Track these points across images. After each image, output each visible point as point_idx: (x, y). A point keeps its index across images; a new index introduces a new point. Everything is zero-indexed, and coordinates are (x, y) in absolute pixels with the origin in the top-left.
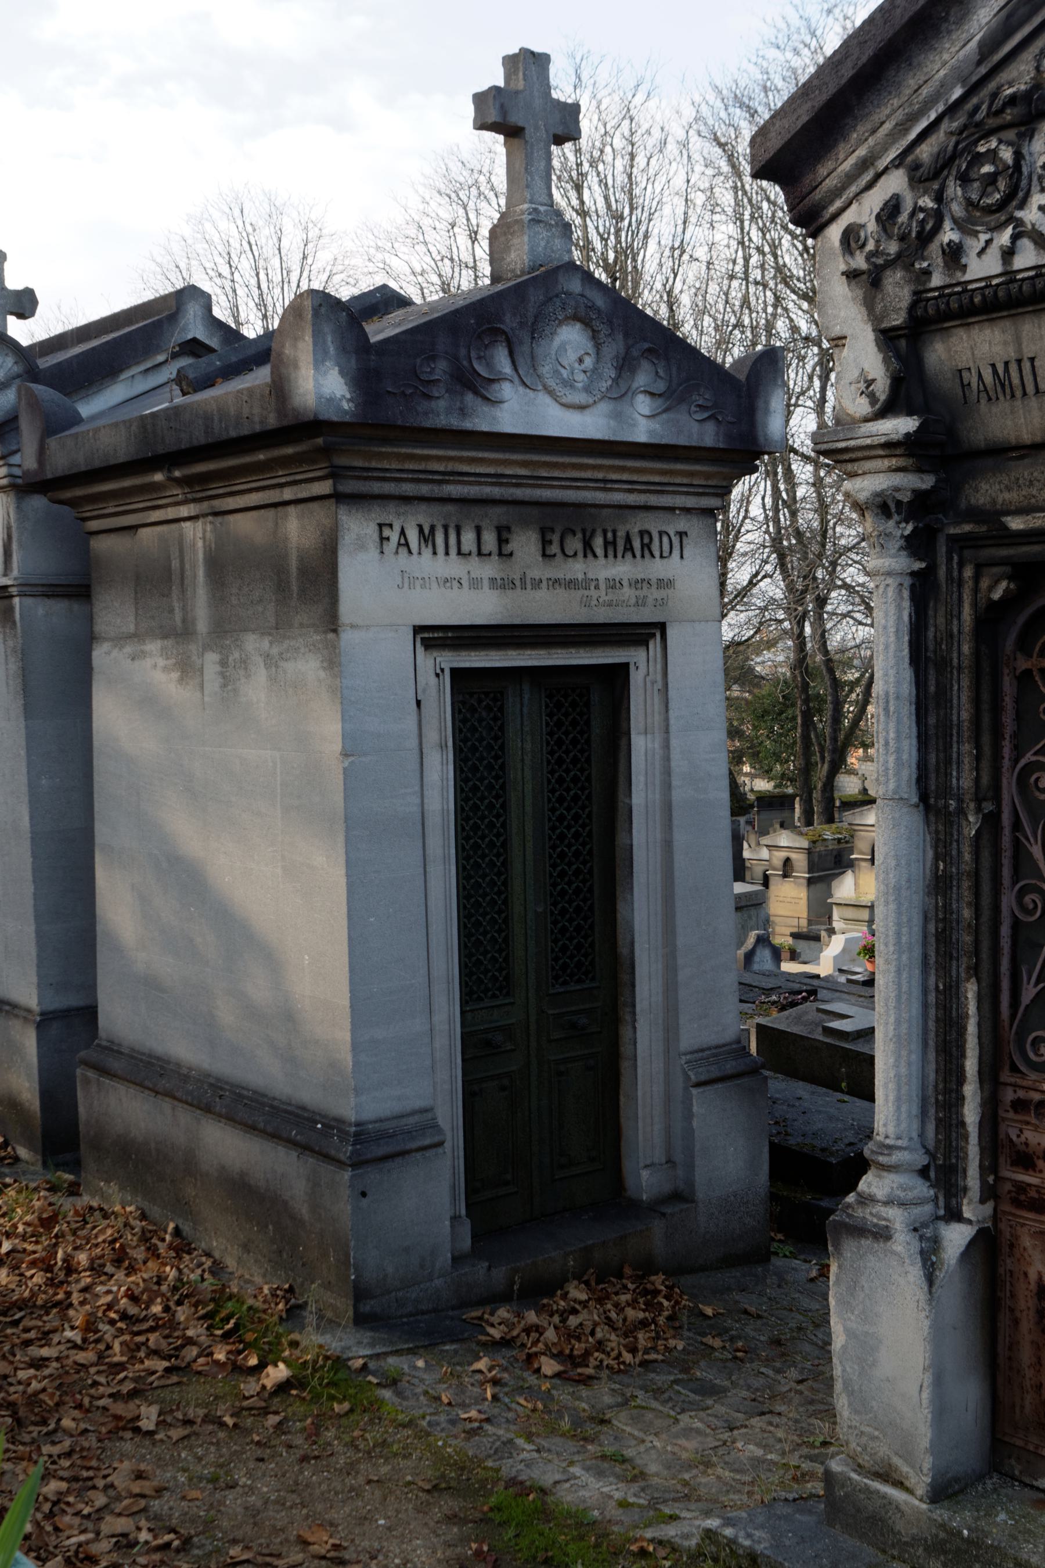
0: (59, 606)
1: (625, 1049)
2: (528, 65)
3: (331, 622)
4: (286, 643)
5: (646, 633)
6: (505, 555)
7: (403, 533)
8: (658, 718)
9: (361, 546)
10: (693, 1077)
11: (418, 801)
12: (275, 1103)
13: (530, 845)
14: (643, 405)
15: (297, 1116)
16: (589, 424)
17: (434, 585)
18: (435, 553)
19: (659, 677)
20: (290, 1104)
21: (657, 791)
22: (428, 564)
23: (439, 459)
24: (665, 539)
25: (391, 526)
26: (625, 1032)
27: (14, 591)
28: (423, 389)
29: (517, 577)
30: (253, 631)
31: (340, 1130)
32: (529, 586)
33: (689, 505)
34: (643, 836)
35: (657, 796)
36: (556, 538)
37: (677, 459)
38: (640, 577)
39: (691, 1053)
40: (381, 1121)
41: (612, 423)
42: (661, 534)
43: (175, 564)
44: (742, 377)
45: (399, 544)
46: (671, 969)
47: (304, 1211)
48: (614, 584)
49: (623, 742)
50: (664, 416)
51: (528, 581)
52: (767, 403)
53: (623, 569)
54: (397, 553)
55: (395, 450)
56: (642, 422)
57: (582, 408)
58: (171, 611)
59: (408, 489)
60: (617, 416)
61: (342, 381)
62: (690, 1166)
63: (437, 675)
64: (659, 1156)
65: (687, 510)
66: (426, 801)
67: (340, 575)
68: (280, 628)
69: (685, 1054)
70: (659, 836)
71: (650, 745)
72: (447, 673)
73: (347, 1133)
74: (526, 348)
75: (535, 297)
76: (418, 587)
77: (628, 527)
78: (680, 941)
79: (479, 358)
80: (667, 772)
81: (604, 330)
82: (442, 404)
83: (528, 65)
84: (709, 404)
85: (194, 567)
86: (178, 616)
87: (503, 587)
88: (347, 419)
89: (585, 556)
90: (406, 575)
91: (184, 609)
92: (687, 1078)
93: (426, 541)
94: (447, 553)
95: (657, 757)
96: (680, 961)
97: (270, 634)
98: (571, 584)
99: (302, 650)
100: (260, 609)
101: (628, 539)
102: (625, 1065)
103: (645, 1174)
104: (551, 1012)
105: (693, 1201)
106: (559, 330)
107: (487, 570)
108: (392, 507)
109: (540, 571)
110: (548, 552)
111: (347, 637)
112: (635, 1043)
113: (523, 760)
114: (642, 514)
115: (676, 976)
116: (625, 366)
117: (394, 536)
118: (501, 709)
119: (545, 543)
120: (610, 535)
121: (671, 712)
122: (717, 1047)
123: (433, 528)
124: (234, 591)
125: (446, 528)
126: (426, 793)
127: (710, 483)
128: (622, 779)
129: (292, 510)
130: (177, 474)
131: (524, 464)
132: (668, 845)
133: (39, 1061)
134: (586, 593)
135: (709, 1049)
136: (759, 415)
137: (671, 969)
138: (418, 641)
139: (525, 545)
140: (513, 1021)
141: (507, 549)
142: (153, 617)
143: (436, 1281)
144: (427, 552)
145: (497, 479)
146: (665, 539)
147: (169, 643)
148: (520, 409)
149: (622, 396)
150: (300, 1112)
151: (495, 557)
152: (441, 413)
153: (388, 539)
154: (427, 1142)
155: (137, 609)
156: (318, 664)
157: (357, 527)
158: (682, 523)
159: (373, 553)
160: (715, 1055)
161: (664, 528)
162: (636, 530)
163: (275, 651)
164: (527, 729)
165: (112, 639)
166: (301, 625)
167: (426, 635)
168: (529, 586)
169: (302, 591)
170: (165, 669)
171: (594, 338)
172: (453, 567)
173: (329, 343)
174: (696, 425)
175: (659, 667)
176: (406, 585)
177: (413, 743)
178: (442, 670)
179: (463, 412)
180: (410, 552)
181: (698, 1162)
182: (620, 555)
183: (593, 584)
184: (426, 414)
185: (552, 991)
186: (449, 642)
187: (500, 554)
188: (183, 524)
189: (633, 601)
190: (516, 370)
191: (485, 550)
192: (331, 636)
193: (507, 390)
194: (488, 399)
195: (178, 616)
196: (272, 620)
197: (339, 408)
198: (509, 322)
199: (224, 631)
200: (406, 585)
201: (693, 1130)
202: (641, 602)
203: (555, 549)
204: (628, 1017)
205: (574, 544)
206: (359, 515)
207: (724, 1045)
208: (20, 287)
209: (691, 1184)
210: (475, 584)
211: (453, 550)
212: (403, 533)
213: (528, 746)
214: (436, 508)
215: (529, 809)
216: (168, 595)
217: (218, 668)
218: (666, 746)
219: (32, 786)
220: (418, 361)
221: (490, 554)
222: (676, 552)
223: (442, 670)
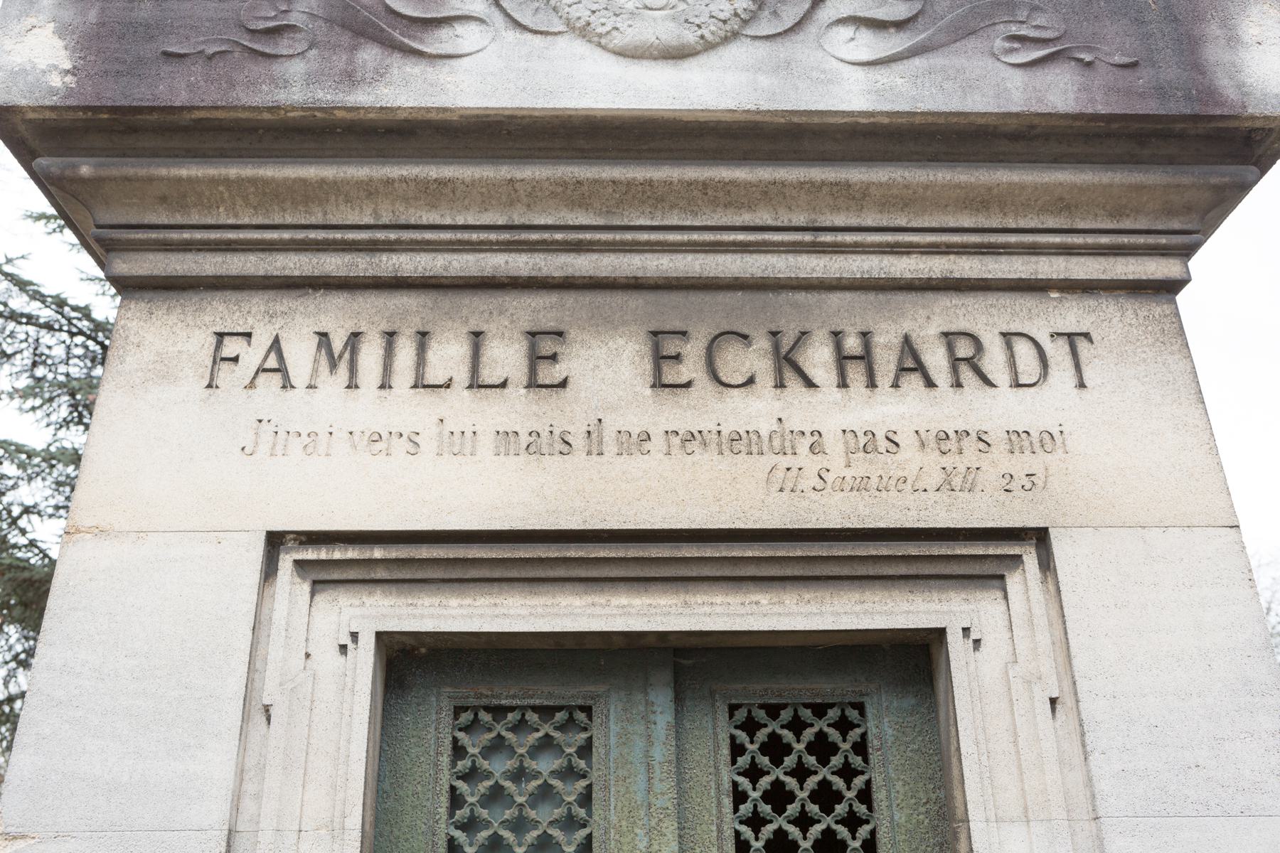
7: (276, 346)
22: (327, 403)
36: (693, 351)
48: (867, 443)
72: (367, 645)
93: (333, 365)
98: (738, 442)
107: (516, 410)
119: (660, 359)
125: (390, 336)
127: (1127, 224)
151: (517, 392)
162: (933, 329)
167: (310, 554)
172: (406, 409)
175: (1044, 639)
176: (264, 448)
182: (884, 380)
186: (381, 574)
189: (936, 478)
200: (264, 448)
203: (691, 368)
205: (753, 359)
221: (503, 385)
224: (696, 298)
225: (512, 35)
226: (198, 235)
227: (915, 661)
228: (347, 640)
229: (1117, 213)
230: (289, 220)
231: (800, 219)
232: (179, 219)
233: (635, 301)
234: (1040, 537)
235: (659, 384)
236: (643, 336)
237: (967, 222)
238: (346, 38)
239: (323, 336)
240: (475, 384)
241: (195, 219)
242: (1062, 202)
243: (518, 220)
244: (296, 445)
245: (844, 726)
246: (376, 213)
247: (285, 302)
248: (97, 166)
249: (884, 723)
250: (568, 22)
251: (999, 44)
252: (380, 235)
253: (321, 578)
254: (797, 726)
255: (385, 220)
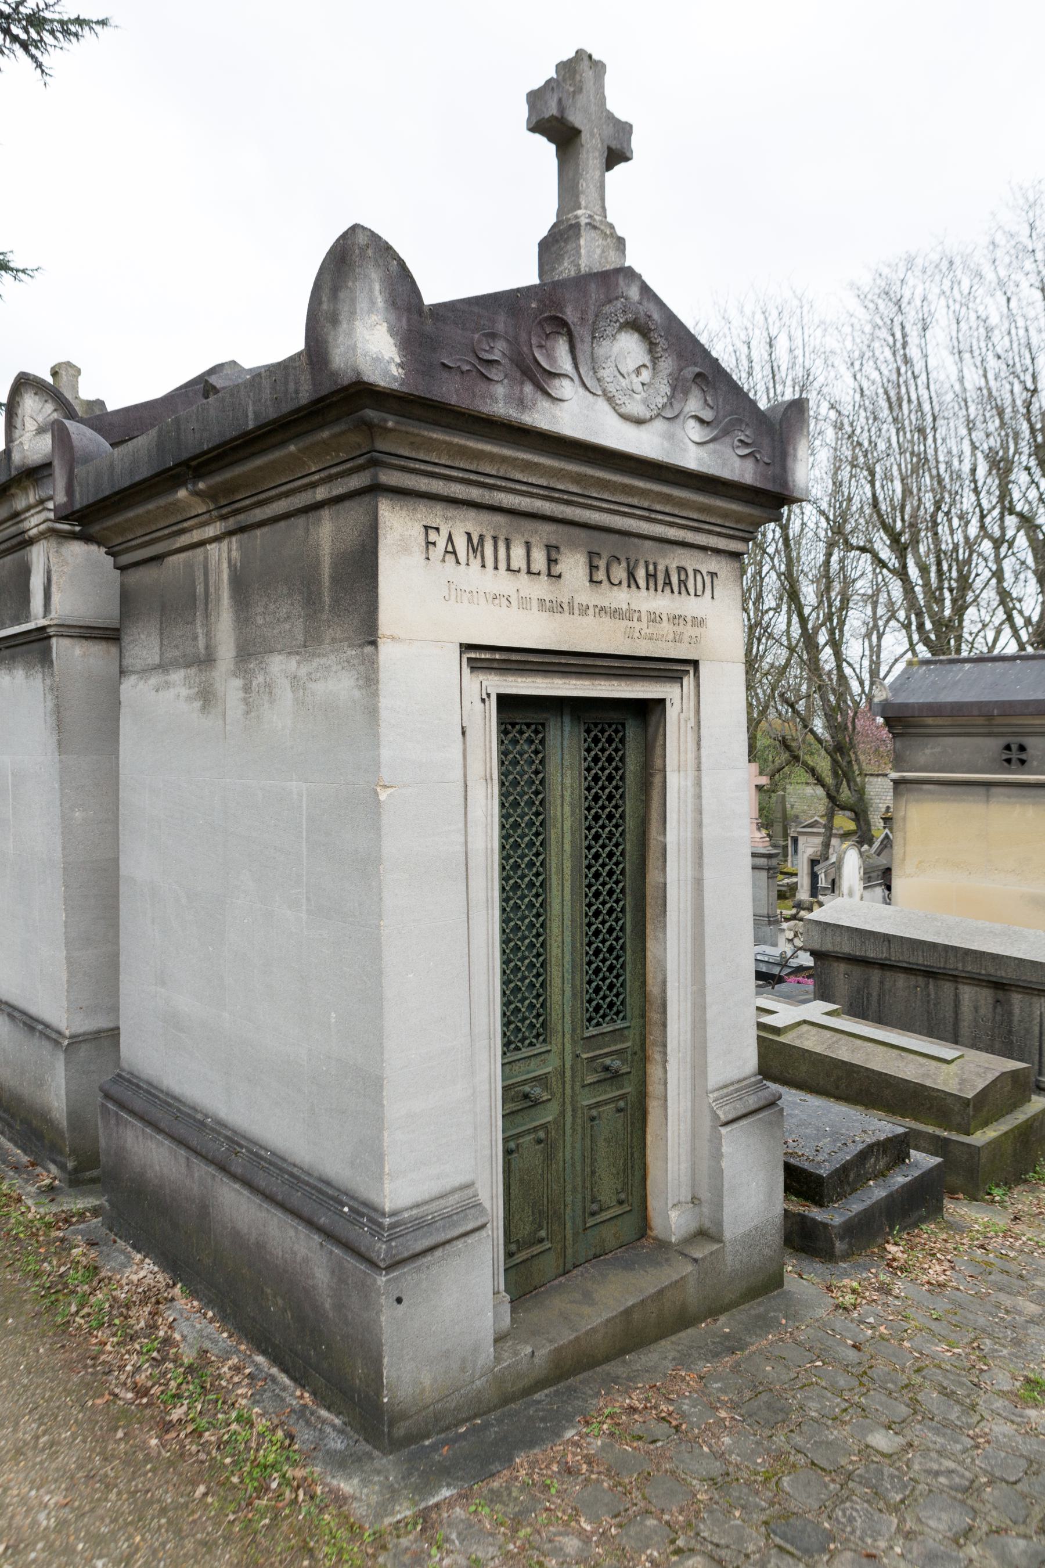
0: (97, 649)
1: (653, 1088)
2: (579, 72)
3: (368, 633)
4: (316, 662)
5: (676, 669)
6: (554, 577)
7: (450, 538)
8: (691, 756)
9: (405, 548)
10: (722, 1116)
11: (463, 839)
12: (295, 1170)
13: (568, 884)
14: (694, 431)
15: (320, 1191)
16: (643, 443)
17: (482, 600)
18: (483, 566)
19: (692, 714)
20: (309, 1174)
21: (689, 829)
22: (475, 577)
23: (492, 458)
24: (699, 577)
25: (437, 529)
26: (654, 1071)
27: (51, 631)
28: (482, 369)
29: (565, 600)
30: (279, 652)
31: (371, 1220)
32: (576, 612)
33: (720, 547)
34: (676, 875)
35: (689, 834)
36: (602, 564)
37: (716, 494)
38: (677, 613)
39: (717, 1090)
40: (417, 1206)
41: (666, 444)
42: (696, 571)
43: (200, 589)
44: (779, 416)
45: (446, 552)
46: (699, 1007)
47: (327, 1306)
48: (655, 618)
49: (657, 779)
50: (711, 445)
51: (576, 606)
52: (795, 449)
53: (662, 603)
54: (443, 561)
55: (447, 438)
56: (689, 448)
57: (639, 422)
58: (195, 638)
59: (458, 490)
60: (671, 437)
61: (392, 341)
62: (719, 1206)
63: (483, 700)
64: (685, 1195)
65: (717, 551)
66: (470, 839)
67: (381, 578)
68: (310, 643)
69: (712, 1092)
70: (690, 873)
71: (683, 783)
72: (494, 698)
73: (380, 1225)
74: (586, 347)
75: (595, 292)
76: (466, 601)
77: (667, 561)
78: (709, 978)
79: (541, 346)
80: (699, 810)
81: (662, 343)
82: (500, 390)
83: (579, 72)
84: (749, 441)
85: (218, 589)
86: (201, 643)
87: (552, 610)
88: (395, 386)
89: (629, 586)
90: (453, 587)
91: (208, 635)
92: (716, 1117)
93: (475, 551)
94: (496, 568)
95: (690, 795)
96: (709, 999)
97: (298, 653)
98: (616, 614)
99: (334, 669)
100: (287, 626)
101: (667, 574)
102: (653, 1107)
103: (673, 1215)
104: (585, 1056)
105: (720, 1241)
106: (618, 336)
107: (540, 589)
108: (439, 508)
109: (586, 596)
110: (595, 579)
111: (386, 650)
112: (666, 1084)
113: (562, 796)
114: (680, 551)
115: (705, 1013)
116: (679, 388)
117: (441, 542)
118: (542, 742)
119: (593, 568)
120: (651, 567)
121: (703, 750)
122: (739, 1081)
123: (481, 537)
124: (260, 610)
125: (495, 539)
126: (470, 830)
127: (739, 526)
128: (654, 815)
129: (326, 513)
130: (201, 485)
131: (578, 479)
132: (698, 883)
133: (67, 1083)
134: (630, 624)
135: (732, 1084)
136: (790, 462)
137: (699, 1007)
138: (464, 660)
139: (573, 566)
140: (550, 1069)
141: (557, 570)
142: (177, 647)
143: (478, 1382)
144: (476, 563)
145: (549, 494)
146: (699, 577)
147: (192, 671)
148: (574, 412)
149: (676, 417)
150: (320, 1185)
151: (544, 578)
152: (499, 401)
153: (434, 544)
154: (470, 1226)
155: (162, 639)
156: (352, 682)
157: (399, 528)
158: (712, 564)
159: (418, 556)
160: (737, 1091)
161: (698, 567)
162: (674, 565)
163: (303, 671)
164: (566, 763)
165: (138, 672)
166: (334, 640)
167: (473, 655)
168: (576, 612)
169: (336, 602)
170: (189, 699)
171: (651, 351)
172: (502, 583)
173: (377, 293)
174: (737, 459)
175: (692, 704)
176: (453, 597)
177: (458, 774)
178: (488, 695)
179: (522, 404)
180: (458, 562)
181: (726, 1201)
182: (660, 588)
183: (636, 615)
184: (483, 397)
185: (587, 1035)
186: (495, 665)
187: (549, 575)
188: (208, 547)
189: (671, 637)
190: (576, 367)
191: (535, 568)
192: (369, 649)
193: (566, 389)
194: (549, 395)
195: (201, 643)
196: (301, 638)
197: (386, 373)
198: (571, 315)
199: (248, 653)
200: (453, 597)
201: (722, 1171)
202: (677, 639)
203: (601, 575)
204: (658, 1057)
205: (619, 573)
206: (404, 513)
207: (745, 1079)
208: (92, 397)
209: (719, 1224)
210: (524, 603)
211: (503, 565)
212: (450, 538)
213: (568, 781)
214: (486, 516)
215: (567, 847)
216: (193, 622)
217: (241, 694)
218: (698, 783)
219: (65, 818)
220: (476, 336)
221: (539, 574)
222: (708, 591)
223: (488, 695)
224: (604, 536)
225: (581, 391)
226: (423, 467)
227: (648, 712)
228: (484, 696)
229: (737, 522)
230: (462, 465)
231: (646, 505)
232: (414, 455)
233: (583, 534)
234: (695, 663)
235: (591, 581)
236: (586, 555)
237: (695, 516)
238: (518, 375)
239: (469, 534)
240: (529, 572)
241: (421, 456)
242: (726, 514)
243: (552, 485)
244: (466, 596)
245: (616, 731)
246: (498, 470)
247: (452, 512)
248: (397, 423)
249: (631, 732)
250: (604, 391)
251: (736, 443)
252: (499, 483)
253: (475, 666)
254: (603, 731)
255: (501, 474)
